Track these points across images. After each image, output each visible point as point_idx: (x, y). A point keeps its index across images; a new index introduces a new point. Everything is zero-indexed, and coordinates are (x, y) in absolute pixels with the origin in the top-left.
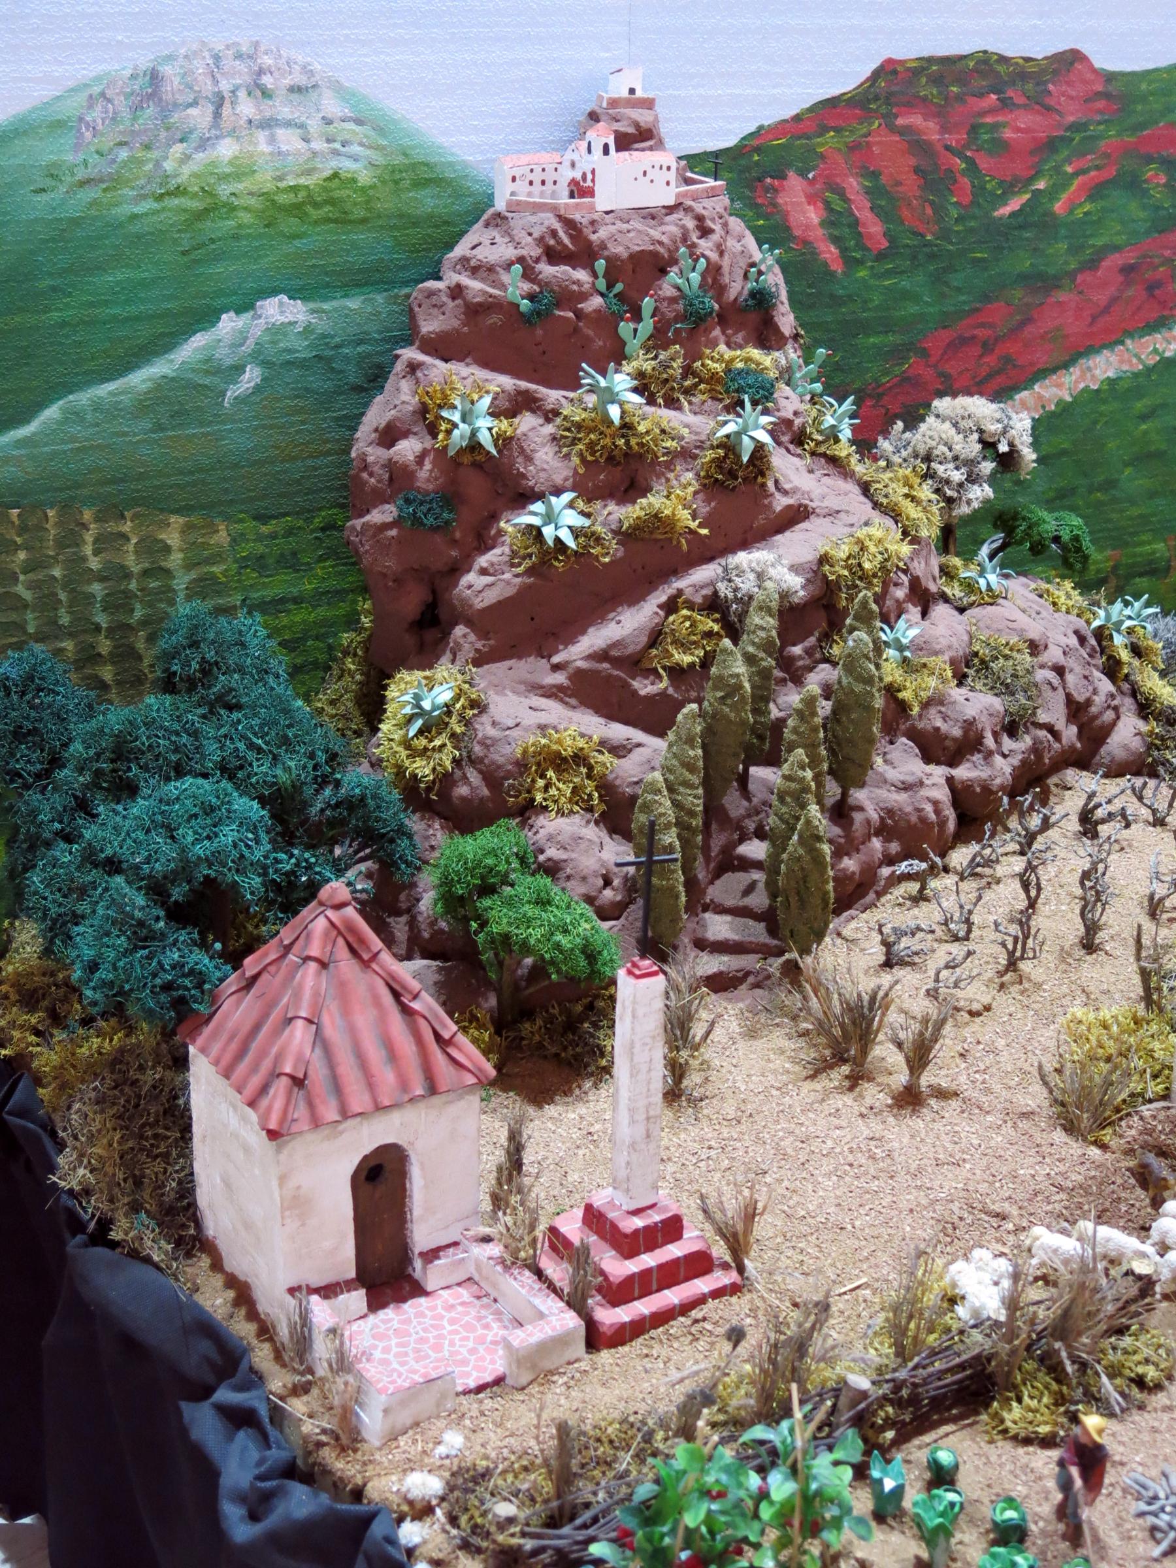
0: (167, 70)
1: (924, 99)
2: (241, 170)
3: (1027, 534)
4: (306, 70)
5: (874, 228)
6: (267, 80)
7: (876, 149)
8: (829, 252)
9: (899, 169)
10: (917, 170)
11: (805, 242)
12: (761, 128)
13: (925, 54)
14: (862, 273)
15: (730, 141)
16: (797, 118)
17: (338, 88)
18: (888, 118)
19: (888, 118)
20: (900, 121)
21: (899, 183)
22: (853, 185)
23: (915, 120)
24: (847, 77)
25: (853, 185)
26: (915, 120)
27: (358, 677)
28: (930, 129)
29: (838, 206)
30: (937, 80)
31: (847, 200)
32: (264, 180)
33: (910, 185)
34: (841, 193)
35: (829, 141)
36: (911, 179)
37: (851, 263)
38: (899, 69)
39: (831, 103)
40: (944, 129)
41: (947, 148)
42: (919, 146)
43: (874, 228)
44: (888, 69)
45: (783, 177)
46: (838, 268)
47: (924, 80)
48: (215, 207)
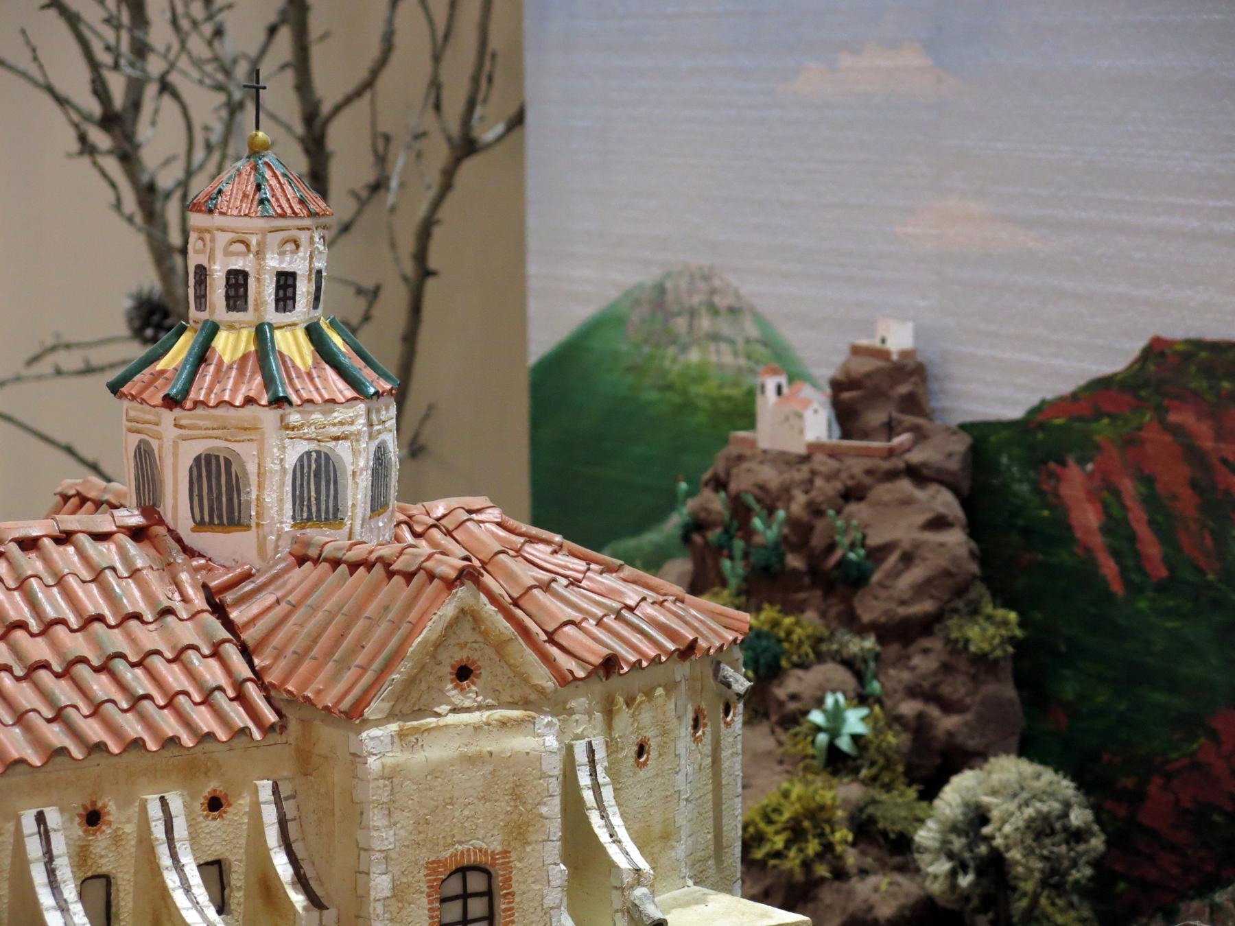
0: (669, 284)
1: (1196, 394)
2: (701, 376)
3: (84, 839)
4: (738, 297)
5: (1152, 548)
6: (717, 300)
7: (1149, 448)
8: (1109, 568)
9: (1174, 478)
10: (1194, 485)
11: (1087, 550)
12: (1043, 402)
13: (1193, 335)
14: (1143, 605)
15: (1015, 413)
16: (1075, 396)
17: (758, 318)
18: (1161, 411)
19: (1161, 411)
20: (1173, 418)
21: (1174, 497)
22: (1128, 487)
23: (1183, 417)
24: (1115, 356)
25: (1128, 487)
26: (1183, 417)
27: (402, 833)
28: (1203, 432)
29: (1116, 512)
30: (1208, 371)
31: (1124, 507)
32: (711, 387)
33: (1187, 504)
34: (1116, 493)
35: (1103, 430)
36: (1186, 494)
37: (1135, 589)
38: (1168, 351)
39: (1102, 385)
40: (1219, 436)
41: (1225, 461)
42: (1193, 454)
43: (1152, 548)
44: (1156, 351)
45: (1063, 463)
46: (1117, 588)
47: (1193, 369)
48: (688, 406)
